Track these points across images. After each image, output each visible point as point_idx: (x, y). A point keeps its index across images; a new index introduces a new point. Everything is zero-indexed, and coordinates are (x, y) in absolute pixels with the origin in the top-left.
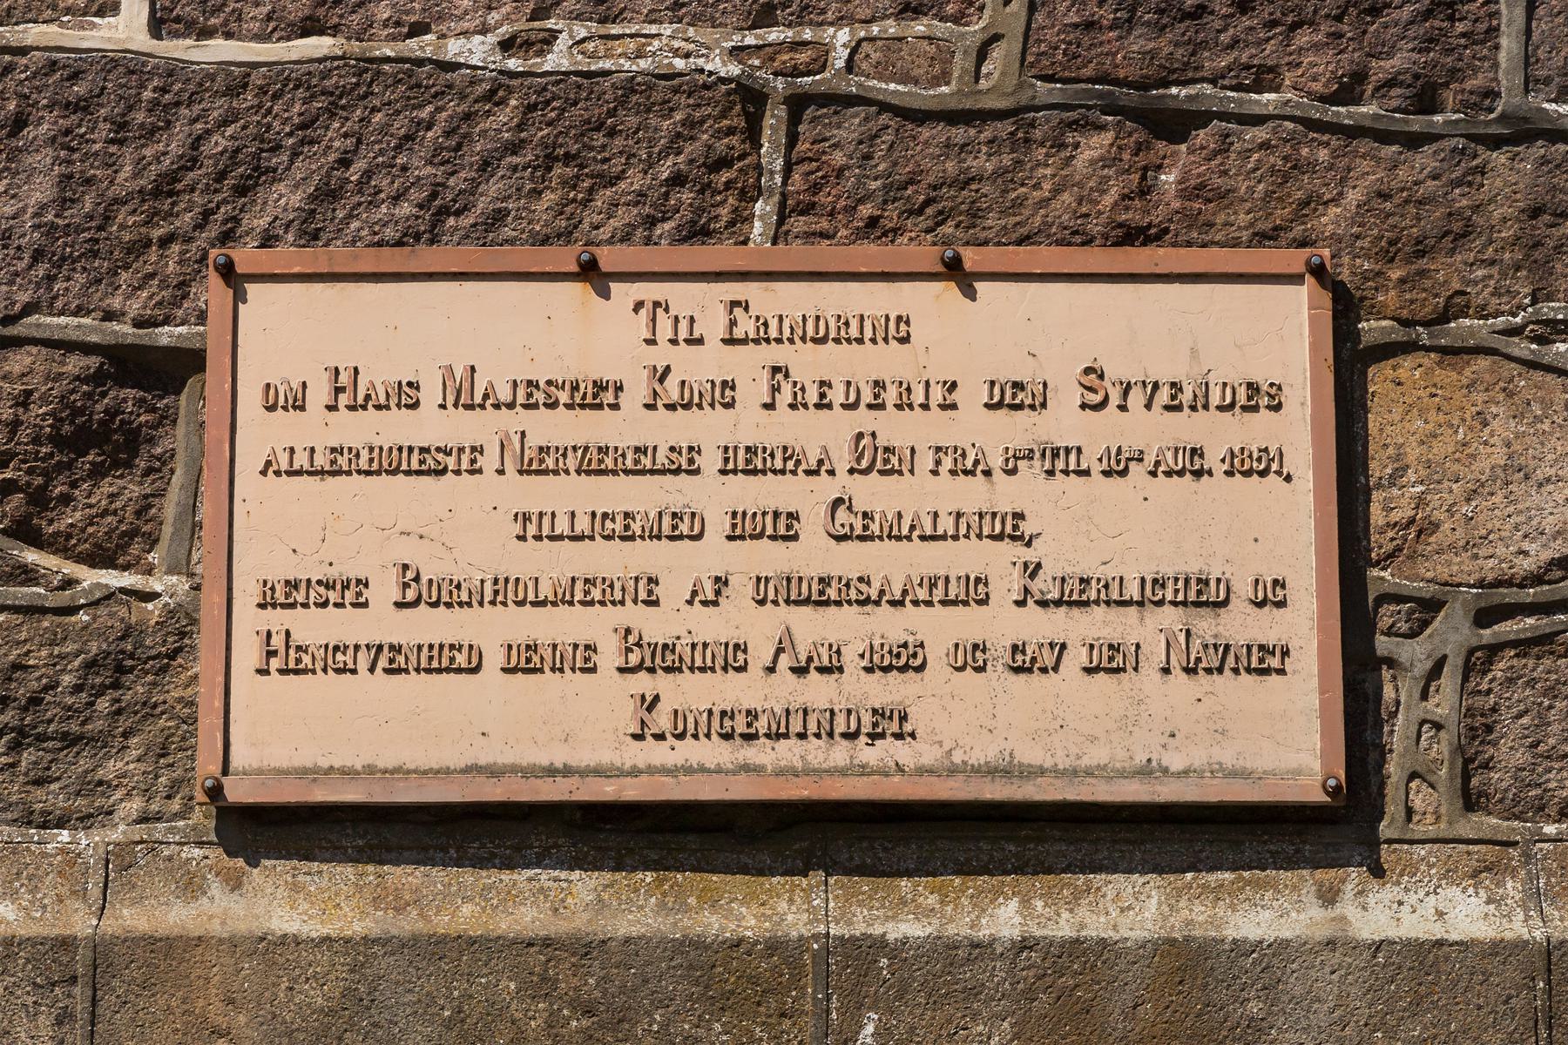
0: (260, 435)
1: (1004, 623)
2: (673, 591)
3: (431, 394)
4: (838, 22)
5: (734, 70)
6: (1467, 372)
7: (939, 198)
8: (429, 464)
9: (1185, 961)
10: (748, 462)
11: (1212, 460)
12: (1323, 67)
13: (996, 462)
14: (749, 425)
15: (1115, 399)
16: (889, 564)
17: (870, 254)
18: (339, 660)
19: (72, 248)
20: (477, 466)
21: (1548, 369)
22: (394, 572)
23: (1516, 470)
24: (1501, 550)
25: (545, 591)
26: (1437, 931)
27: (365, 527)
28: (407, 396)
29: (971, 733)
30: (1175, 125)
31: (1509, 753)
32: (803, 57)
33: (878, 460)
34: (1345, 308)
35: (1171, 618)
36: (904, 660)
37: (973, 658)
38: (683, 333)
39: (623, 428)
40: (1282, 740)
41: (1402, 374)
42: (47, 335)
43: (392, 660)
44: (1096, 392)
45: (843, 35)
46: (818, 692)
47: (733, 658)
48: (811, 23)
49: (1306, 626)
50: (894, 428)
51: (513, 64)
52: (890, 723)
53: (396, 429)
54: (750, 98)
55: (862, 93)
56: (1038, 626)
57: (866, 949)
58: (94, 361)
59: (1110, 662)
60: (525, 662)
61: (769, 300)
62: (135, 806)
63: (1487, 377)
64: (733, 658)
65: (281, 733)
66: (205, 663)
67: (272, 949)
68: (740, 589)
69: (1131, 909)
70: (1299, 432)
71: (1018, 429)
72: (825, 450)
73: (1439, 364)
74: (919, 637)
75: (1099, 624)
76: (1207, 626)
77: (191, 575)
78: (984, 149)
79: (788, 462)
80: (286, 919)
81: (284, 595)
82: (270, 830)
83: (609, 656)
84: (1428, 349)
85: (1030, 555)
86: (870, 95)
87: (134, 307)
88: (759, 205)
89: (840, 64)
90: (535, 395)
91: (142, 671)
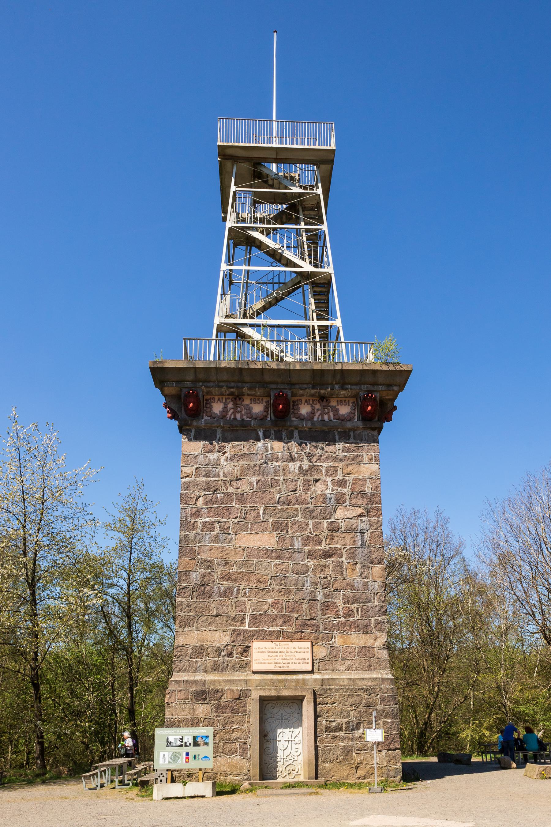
0: (254, 651)
1: (294, 661)
9: (304, 680)
10: (281, 652)
12: (311, 629)
14: (280, 650)
16: (288, 658)
19: (244, 640)
23: (321, 652)
27: (260, 656)
28: (262, 649)
29: (292, 667)
30: (303, 632)
31: (321, 668)
33: (287, 652)
34: (312, 643)
36: (289, 663)
37: (292, 663)
39: (273, 650)
40: (309, 668)
43: (262, 663)
44: (299, 648)
46: (284, 665)
47: (280, 663)
49: (310, 661)
50: (288, 650)
52: (288, 667)
54: (280, 631)
56: (296, 661)
57: (287, 679)
59: (300, 663)
64: (280, 663)
65: (256, 668)
66: (251, 663)
67: (256, 680)
69: (301, 677)
71: (295, 650)
75: (299, 661)
80: (256, 678)
82: (254, 673)
90: (269, 648)
91: (248, 663)
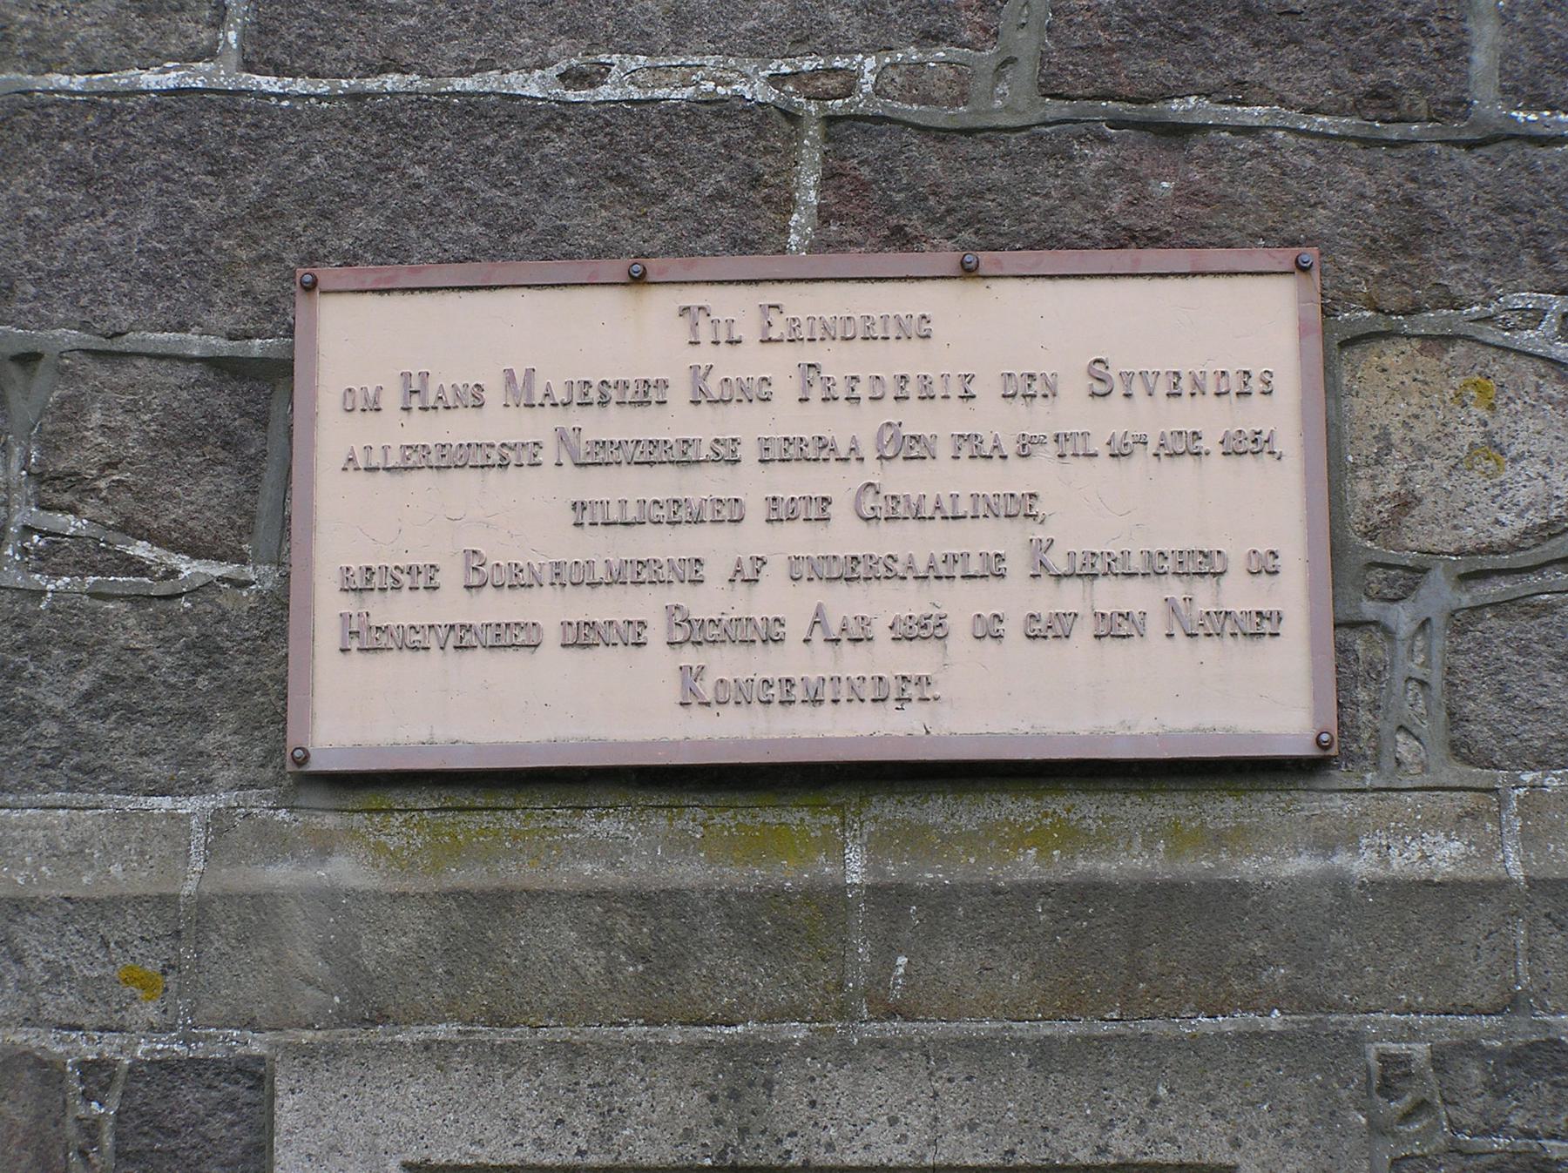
2: (717, 572)
3: (494, 394)
4: (867, 50)
5: (772, 95)
6: (1447, 358)
7: (922, 198)
8: (501, 458)
11: (1209, 443)
13: (1010, 448)
14: (788, 418)
15: (1119, 390)
16: (918, 543)
17: (894, 261)
18: (411, 642)
20: (537, 460)
21: (1519, 353)
22: (460, 559)
24: (1479, 522)
25: (600, 573)
26: (1423, 871)
32: (833, 83)
33: (914, 449)
35: (1176, 589)
36: (928, 630)
37: (990, 631)
38: (723, 338)
39: (676, 422)
40: (1270, 698)
41: (1387, 361)
42: (151, 349)
43: (462, 639)
44: (1101, 381)
45: (870, 63)
48: (839, 52)
49: (1295, 595)
50: (915, 419)
51: (571, 96)
53: (457, 428)
55: (887, 114)
56: (1049, 599)
58: (194, 373)
59: (1116, 628)
60: (583, 637)
61: (803, 302)
62: (232, 773)
63: (1464, 362)
65: (354, 709)
68: (776, 572)
70: (1284, 415)
72: (996, 438)
73: (1421, 351)
74: (943, 612)
75: (1109, 596)
76: (1204, 596)
77: (280, 564)
78: (1000, 162)
79: (823, 451)
81: (361, 584)
83: (656, 635)
84: (1409, 337)
85: (1040, 533)
86: (896, 116)
87: (228, 322)
88: (795, 217)
89: (867, 88)
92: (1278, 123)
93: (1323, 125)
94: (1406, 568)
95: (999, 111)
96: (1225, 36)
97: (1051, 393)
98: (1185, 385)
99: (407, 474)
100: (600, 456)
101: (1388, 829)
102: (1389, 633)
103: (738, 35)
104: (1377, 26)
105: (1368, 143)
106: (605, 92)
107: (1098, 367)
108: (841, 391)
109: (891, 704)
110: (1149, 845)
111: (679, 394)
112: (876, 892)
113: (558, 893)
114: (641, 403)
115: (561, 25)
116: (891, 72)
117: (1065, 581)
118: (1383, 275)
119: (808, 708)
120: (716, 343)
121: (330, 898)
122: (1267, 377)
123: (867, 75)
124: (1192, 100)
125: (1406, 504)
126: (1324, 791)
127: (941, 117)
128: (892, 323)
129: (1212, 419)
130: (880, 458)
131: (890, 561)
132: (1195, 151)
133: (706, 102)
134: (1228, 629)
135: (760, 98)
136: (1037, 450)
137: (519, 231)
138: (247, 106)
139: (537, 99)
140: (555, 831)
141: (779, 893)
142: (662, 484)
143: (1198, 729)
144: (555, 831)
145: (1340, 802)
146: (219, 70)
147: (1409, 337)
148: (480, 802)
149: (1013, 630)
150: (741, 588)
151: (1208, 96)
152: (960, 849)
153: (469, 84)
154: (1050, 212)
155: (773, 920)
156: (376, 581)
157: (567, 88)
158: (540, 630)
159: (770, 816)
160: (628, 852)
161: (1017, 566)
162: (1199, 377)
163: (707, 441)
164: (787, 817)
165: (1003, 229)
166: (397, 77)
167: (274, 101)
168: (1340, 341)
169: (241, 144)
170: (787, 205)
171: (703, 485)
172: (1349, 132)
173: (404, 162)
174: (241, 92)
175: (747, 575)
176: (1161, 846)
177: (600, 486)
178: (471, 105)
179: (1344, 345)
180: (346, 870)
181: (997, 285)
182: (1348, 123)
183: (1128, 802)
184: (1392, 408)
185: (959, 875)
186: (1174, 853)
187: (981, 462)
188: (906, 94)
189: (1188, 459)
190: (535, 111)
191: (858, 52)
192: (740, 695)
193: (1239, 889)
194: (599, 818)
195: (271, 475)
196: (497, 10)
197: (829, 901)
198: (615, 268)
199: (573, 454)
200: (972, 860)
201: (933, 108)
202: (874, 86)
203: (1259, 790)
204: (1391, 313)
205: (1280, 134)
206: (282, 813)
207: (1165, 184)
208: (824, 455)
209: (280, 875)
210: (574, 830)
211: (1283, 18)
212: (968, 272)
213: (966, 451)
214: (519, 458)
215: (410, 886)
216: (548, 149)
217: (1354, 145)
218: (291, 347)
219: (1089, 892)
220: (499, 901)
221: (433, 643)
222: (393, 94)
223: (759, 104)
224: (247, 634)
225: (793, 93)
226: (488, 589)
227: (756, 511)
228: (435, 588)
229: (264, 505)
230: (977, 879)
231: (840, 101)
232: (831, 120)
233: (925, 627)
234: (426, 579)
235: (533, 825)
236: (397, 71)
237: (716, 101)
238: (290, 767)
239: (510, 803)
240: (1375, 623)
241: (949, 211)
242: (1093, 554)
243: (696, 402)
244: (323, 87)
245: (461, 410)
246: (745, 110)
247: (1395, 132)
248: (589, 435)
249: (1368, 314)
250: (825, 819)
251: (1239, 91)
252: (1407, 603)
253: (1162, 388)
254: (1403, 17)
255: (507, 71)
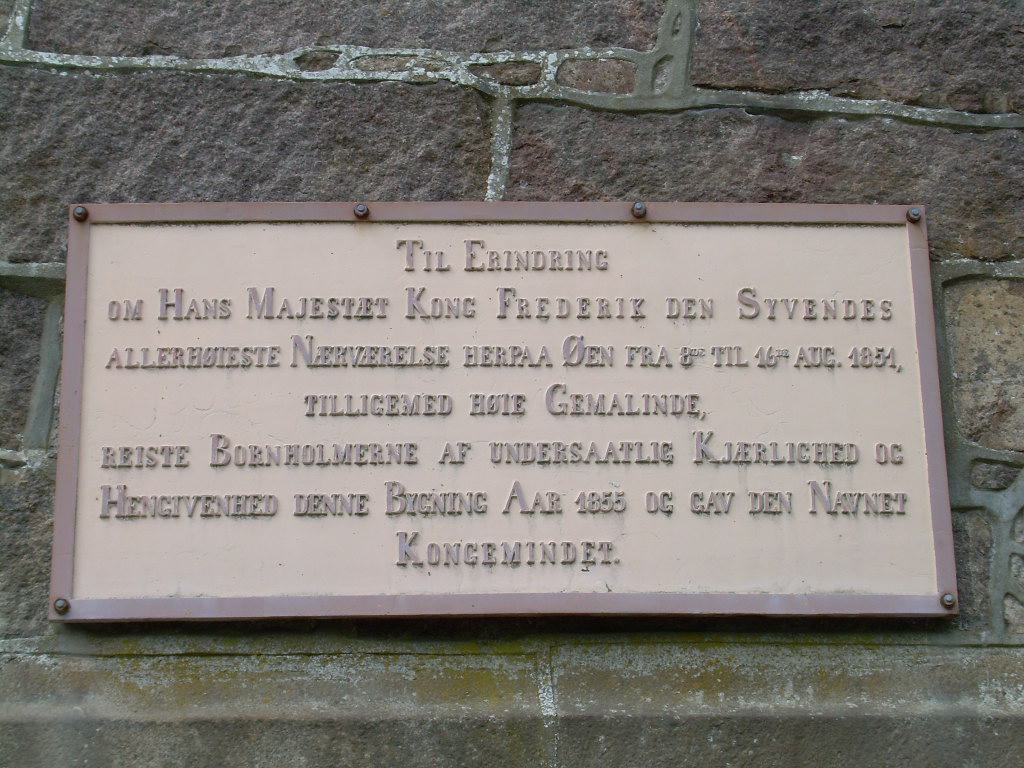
2: (428, 455)
3: (240, 307)
4: (549, 48)
11: (842, 356)
14: (488, 331)
18: (165, 510)
32: (522, 72)
33: (590, 358)
35: (818, 475)
36: (606, 506)
38: (435, 266)
40: (905, 569)
41: (982, 298)
43: (208, 508)
45: (553, 57)
49: (918, 479)
50: (596, 334)
51: (305, 75)
55: (567, 97)
59: (768, 507)
60: (313, 508)
61: (502, 240)
65: (115, 566)
68: (480, 456)
70: (904, 333)
73: (1010, 290)
75: (761, 479)
76: (843, 481)
78: (660, 137)
79: (519, 358)
81: (121, 460)
83: (378, 505)
84: (999, 279)
85: (705, 428)
88: (491, 176)
89: (550, 77)
92: (885, 111)
93: (923, 114)
94: (1006, 463)
95: (660, 97)
96: (841, 44)
97: (708, 314)
98: (820, 312)
99: (162, 372)
100: (327, 360)
101: (1002, 678)
102: (993, 517)
103: (444, 33)
104: (964, 37)
105: (958, 129)
106: (333, 73)
107: (748, 296)
108: (534, 311)
109: (579, 566)
110: (799, 688)
111: (399, 308)
112: (570, 724)
113: (290, 723)
114: (363, 317)
115: (297, 21)
116: (570, 66)
117: (723, 466)
118: (977, 230)
119: (509, 570)
120: (428, 270)
121: (88, 728)
122: (887, 305)
123: (550, 67)
124: (815, 93)
125: (1002, 412)
126: (947, 646)
127: (612, 100)
128: (576, 258)
129: (845, 338)
130: (566, 364)
131: (576, 449)
132: (818, 133)
133: (418, 84)
134: (863, 507)
135: (462, 81)
136: (698, 361)
137: (261, 181)
138: (32, 74)
139: (277, 77)
140: (286, 674)
141: (483, 724)
142: (384, 383)
143: (838, 592)
144: (286, 674)
145: (959, 656)
146: (7, 45)
147: (999, 279)
148: (220, 648)
149: (682, 504)
150: (448, 468)
151: (828, 90)
152: (638, 691)
153: (221, 64)
154: (704, 175)
155: (480, 748)
156: (134, 459)
157: (302, 69)
158: (276, 503)
159: (472, 663)
160: (350, 691)
161: (685, 452)
162: (832, 305)
163: (421, 350)
164: (485, 663)
165: (664, 189)
166: (159, 57)
167: (54, 71)
168: (945, 284)
169: (26, 106)
170: (484, 167)
171: (413, 385)
172: (944, 120)
173: (164, 124)
174: (26, 64)
175: (455, 458)
176: (810, 690)
177: (324, 383)
178: (224, 78)
179: (947, 284)
180: (103, 705)
181: (661, 230)
182: (943, 113)
183: (780, 654)
184: (987, 336)
185: (638, 710)
186: (822, 695)
187: (650, 369)
188: (581, 82)
189: (824, 370)
190: (275, 86)
191: (543, 49)
192: (445, 558)
193: (883, 724)
194: (324, 663)
195: (42, 376)
196: (245, 8)
197: (526, 729)
198: (345, 209)
199: (308, 358)
200: (649, 700)
201: (603, 94)
202: (556, 76)
203: (890, 645)
204: (985, 260)
205: (887, 121)
206: (43, 658)
207: (795, 158)
208: (519, 361)
209: (40, 709)
210: (302, 673)
211: (888, 31)
212: (640, 218)
213: (639, 359)
214: (260, 360)
215: (160, 716)
216: (286, 116)
217: (947, 131)
218: (63, 270)
219: (754, 724)
220: (239, 729)
221: (184, 513)
222: (157, 69)
223: (462, 86)
224: (17, 507)
225: (490, 79)
226: (232, 468)
227: (463, 406)
228: (186, 466)
229: (35, 401)
230: (656, 714)
231: (528, 87)
232: (520, 102)
233: (605, 502)
234: (177, 458)
235: (266, 667)
236: (160, 53)
237: (427, 83)
238: (53, 616)
239: (246, 650)
240: (981, 508)
241: (618, 175)
242: (746, 445)
243: (411, 318)
244: (97, 62)
245: (211, 321)
246: (450, 91)
247: (981, 121)
248: (320, 343)
249: (965, 260)
250: (520, 666)
251: (854, 88)
252: (1008, 492)
253: (802, 312)
254: (984, 31)
255: (252, 55)
